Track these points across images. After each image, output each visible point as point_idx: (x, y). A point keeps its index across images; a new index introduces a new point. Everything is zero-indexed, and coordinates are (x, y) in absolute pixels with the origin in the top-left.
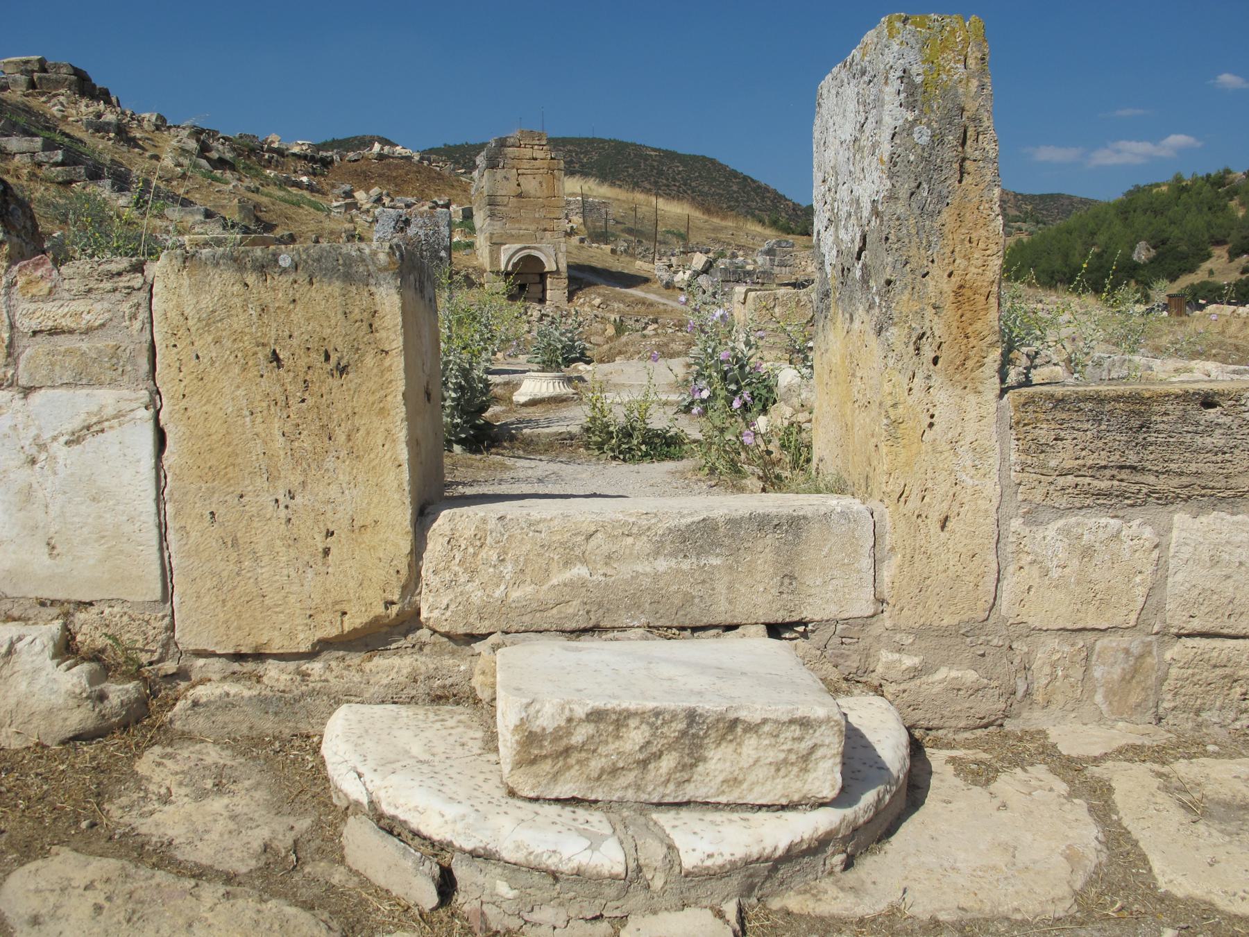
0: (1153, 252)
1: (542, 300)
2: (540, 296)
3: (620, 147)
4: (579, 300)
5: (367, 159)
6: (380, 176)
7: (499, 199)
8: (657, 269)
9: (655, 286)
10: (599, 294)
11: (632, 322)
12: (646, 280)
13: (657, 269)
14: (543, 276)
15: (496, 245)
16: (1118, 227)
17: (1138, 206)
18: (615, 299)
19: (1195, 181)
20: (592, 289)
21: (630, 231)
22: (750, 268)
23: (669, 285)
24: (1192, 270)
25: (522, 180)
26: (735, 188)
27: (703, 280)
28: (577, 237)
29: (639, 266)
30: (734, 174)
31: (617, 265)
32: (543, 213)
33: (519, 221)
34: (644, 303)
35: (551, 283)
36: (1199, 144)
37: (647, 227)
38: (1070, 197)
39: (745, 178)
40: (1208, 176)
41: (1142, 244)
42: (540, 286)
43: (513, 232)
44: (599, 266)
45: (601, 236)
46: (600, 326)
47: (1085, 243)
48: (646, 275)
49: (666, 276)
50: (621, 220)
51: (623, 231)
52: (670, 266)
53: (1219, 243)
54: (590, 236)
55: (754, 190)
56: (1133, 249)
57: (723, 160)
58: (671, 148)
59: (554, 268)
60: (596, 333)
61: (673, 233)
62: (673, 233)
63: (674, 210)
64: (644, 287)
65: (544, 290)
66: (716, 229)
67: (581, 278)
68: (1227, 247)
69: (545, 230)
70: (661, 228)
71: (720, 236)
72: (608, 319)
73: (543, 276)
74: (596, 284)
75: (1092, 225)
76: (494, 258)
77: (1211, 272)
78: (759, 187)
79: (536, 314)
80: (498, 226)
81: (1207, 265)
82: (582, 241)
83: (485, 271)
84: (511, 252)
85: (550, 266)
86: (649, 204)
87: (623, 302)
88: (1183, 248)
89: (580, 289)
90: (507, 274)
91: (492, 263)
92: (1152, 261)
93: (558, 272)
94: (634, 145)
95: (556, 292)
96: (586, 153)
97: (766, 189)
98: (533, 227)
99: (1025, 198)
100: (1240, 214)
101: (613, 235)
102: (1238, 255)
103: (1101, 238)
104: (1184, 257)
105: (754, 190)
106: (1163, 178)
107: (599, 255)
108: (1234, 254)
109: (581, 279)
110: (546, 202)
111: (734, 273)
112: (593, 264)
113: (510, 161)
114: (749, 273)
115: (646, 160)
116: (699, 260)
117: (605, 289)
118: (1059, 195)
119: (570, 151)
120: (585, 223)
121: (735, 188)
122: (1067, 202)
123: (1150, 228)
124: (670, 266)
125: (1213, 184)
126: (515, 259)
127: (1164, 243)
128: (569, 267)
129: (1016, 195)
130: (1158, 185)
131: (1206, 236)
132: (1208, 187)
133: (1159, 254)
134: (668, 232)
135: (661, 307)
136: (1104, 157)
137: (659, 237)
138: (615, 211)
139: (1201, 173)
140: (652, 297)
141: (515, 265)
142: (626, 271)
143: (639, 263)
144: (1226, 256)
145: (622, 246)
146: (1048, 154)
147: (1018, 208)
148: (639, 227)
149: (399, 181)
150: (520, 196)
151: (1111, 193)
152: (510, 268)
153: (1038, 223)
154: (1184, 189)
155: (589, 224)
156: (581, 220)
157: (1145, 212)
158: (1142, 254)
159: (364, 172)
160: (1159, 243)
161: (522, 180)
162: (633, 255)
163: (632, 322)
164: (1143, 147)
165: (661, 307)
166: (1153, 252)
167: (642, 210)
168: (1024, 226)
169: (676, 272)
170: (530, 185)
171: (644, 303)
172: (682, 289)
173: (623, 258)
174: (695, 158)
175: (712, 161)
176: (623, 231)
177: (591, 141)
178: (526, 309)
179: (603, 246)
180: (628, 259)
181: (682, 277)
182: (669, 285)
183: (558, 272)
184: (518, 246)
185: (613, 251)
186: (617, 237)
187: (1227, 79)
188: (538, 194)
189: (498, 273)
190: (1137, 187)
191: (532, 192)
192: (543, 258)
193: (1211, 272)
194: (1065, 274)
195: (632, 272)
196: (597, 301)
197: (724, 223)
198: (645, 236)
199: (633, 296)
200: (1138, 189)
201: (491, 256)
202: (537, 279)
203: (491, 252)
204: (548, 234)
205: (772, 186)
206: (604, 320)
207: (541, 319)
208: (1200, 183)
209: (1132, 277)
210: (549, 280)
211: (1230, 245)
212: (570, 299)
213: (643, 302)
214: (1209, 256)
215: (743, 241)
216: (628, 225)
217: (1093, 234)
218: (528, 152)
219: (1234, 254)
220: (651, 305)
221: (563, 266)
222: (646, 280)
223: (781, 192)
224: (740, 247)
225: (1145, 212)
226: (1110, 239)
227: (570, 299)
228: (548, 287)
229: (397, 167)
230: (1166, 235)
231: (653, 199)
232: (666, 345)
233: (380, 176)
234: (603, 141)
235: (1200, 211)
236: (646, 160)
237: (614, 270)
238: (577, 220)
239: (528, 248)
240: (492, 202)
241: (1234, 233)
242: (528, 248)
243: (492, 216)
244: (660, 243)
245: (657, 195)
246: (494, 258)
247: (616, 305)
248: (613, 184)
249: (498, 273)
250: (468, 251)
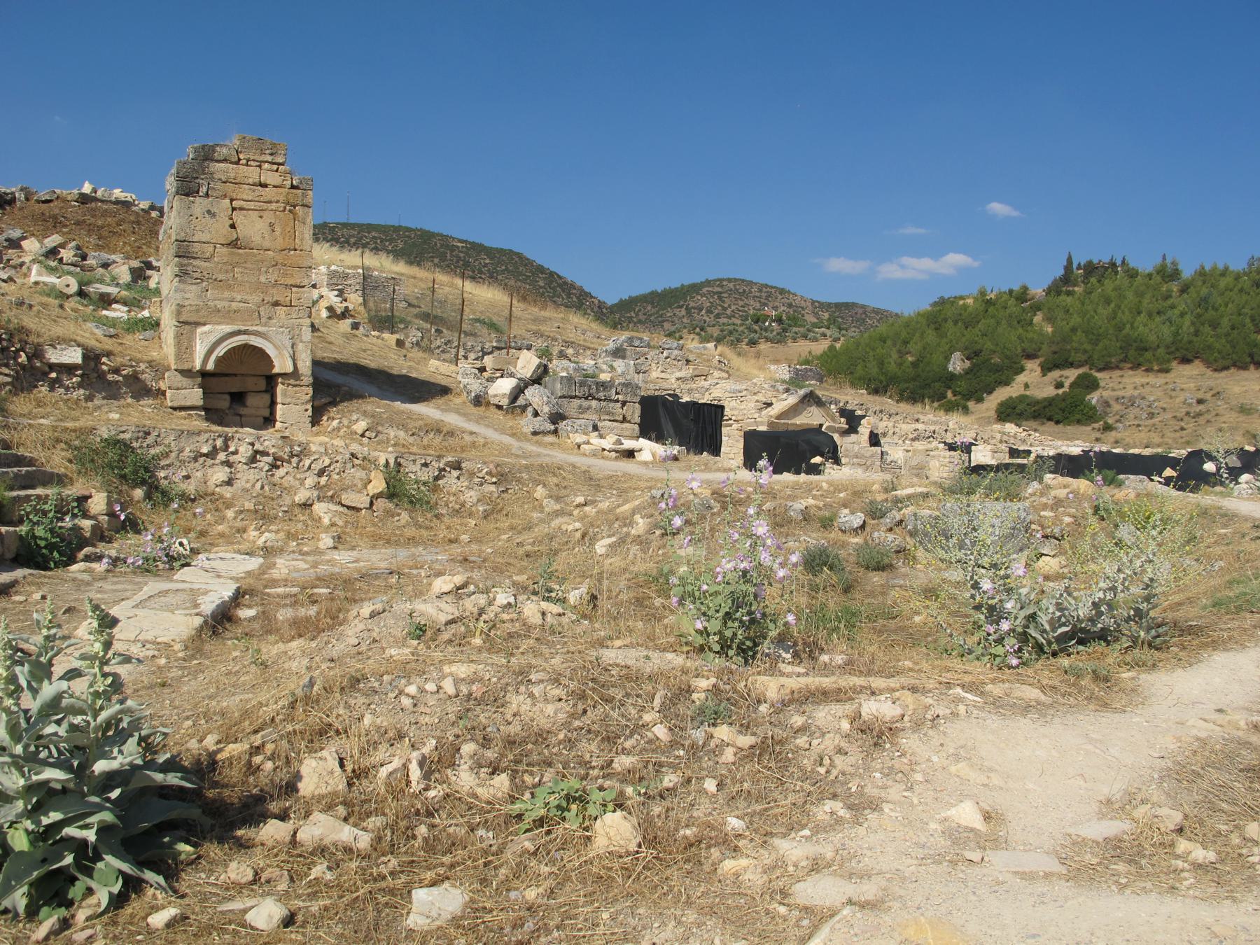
0: (968, 364)
1: (269, 421)
2: (266, 413)
3: (426, 236)
4: (331, 422)
5: (65, 201)
6: (77, 223)
7: (196, 248)
8: (461, 374)
9: (458, 401)
10: (365, 413)
11: (416, 468)
12: (444, 391)
13: (461, 374)
14: (271, 381)
15: (187, 325)
16: (931, 336)
17: (942, 316)
18: (391, 423)
19: (1000, 295)
20: (355, 404)
21: (426, 317)
22: (605, 377)
23: (479, 401)
24: (1007, 383)
25: (239, 218)
26: (541, 283)
27: (533, 395)
28: (349, 321)
29: (434, 368)
30: (541, 269)
31: (399, 364)
32: (273, 275)
33: (230, 288)
34: (439, 431)
35: (285, 394)
36: (976, 264)
37: (453, 315)
38: (863, 306)
39: (552, 274)
40: (1011, 292)
41: (957, 355)
42: (267, 397)
43: (220, 305)
44: (373, 365)
45: (385, 322)
46: (361, 474)
47: (899, 352)
48: (444, 382)
49: (475, 386)
50: (415, 302)
51: (416, 316)
52: (482, 370)
53: (1030, 356)
54: (370, 321)
55: (560, 286)
56: (948, 359)
57: (529, 255)
58: (478, 240)
59: (290, 369)
60: (352, 487)
61: (483, 322)
62: (483, 322)
63: (486, 296)
64: (440, 401)
65: (273, 404)
66: (536, 320)
67: (335, 385)
68: (1038, 361)
69: (276, 304)
70: (468, 315)
71: (543, 328)
72: (374, 462)
73: (271, 381)
74: (361, 397)
75: (904, 335)
76: (183, 346)
77: (1026, 386)
78: (565, 283)
79: (245, 451)
80: (192, 293)
81: (1021, 378)
82: (355, 326)
83: (168, 369)
84: (213, 339)
85: (282, 364)
86: (452, 285)
87: (404, 427)
88: (996, 360)
89: (334, 403)
90: (204, 374)
91: (179, 357)
92: (968, 372)
93: (295, 374)
94: (442, 235)
95: (292, 406)
96: (391, 241)
97: (573, 286)
98: (255, 298)
99: (822, 305)
100: (1050, 330)
101: (403, 321)
102: (1050, 370)
103: (915, 347)
104: (998, 369)
105: (560, 286)
106: (967, 293)
107: (377, 349)
108: (1046, 369)
109: (338, 386)
110: (279, 258)
111: (582, 384)
112: (364, 362)
113: (219, 185)
114: (604, 386)
115: (452, 251)
116: (527, 363)
117: (377, 405)
118: (854, 305)
119: (374, 238)
120: (365, 303)
121: (541, 283)
122: (860, 311)
123: (964, 339)
124: (482, 370)
125: (1017, 299)
126: (220, 351)
127: (977, 354)
128: (316, 363)
129: (813, 302)
130: (962, 298)
131: (1019, 350)
132: (1012, 302)
133: (974, 365)
134: (477, 320)
135: (467, 438)
136: (891, 271)
137: (465, 327)
138: (404, 290)
139: (1005, 289)
140: (453, 420)
141: (219, 361)
142: (414, 375)
143: (434, 363)
144: (1039, 369)
145: (414, 335)
146: (838, 265)
147: (816, 314)
148: (438, 312)
149: (104, 233)
150: (234, 244)
151: (911, 305)
152: (210, 366)
153: (841, 329)
154: (989, 303)
155: (371, 304)
156: (361, 300)
157: (956, 323)
158: (957, 364)
159: (55, 217)
160: (972, 354)
161: (239, 218)
162: (429, 350)
163: (416, 468)
164: (926, 263)
165: (467, 438)
166: (968, 364)
167: (442, 292)
168: (828, 332)
169: (491, 380)
170: (253, 227)
171: (439, 431)
172: (499, 407)
173: (416, 354)
174: (501, 251)
175: (519, 255)
176: (416, 316)
177: (397, 229)
178: (227, 440)
179: (386, 335)
180: (421, 354)
181: (504, 386)
182: (479, 401)
183: (295, 374)
184: (228, 329)
185: (400, 343)
186: (407, 324)
187: (997, 208)
188: (267, 244)
189: (187, 373)
190: (942, 298)
191: (257, 240)
192: (270, 350)
193: (1026, 386)
194: (881, 382)
195: (422, 377)
196: (361, 426)
197: (546, 314)
198: (443, 324)
199: (421, 417)
200: (942, 302)
201: (178, 344)
202: (262, 384)
203: (178, 336)
204: (281, 311)
205: (579, 284)
206: (367, 463)
207: (253, 460)
208: (1006, 297)
209: (950, 388)
210: (280, 388)
211: (1042, 359)
212: (315, 420)
213: (437, 428)
214: (1022, 369)
215: (572, 336)
216: (424, 309)
217: (906, 343)
218: (252, 174)
219: (1046, 369)
220: (451, 433)
221: (305, 366)
222: (444, 391)
223: (587, 289)
224: (568, 344)
225: (956, 323)
226: (925, 348)
227: (315, 420)
228: (279, 400)
229: (105, 213)
230: (978, 347)
231: (459, 282)
232: (495, 700)
233: (77, 223)
234: (409, 230)
235: (1010, 325)
236: (452, 251)
237: (395, 372)
238: (355, 299)
239: (245, 332)
240: (184, 252)
241: (1045, 347)
242: (245, 332)
243: (182, 274)
244: (467, 334)
245: (463, 277)
246: (183, 346)
247: (392, 433)
248: (410, 263)
249: (187, 373)
250: (149, 334)
